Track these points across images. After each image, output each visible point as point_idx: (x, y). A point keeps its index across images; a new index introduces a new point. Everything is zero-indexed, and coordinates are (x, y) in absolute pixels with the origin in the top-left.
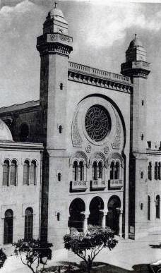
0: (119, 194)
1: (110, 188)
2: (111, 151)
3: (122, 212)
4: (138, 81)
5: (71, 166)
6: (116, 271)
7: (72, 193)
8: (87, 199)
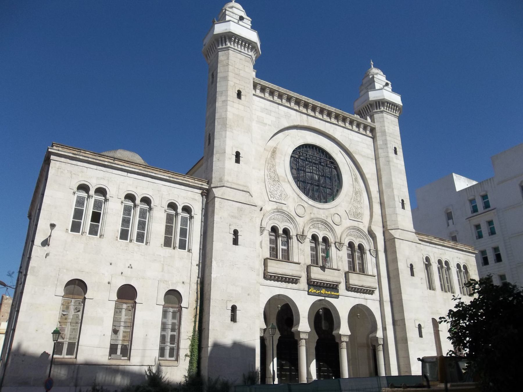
0: (371, 303)
1: (349, 288)
2: (347, 223)
3: (381, 342)
4: (383, 117)
5: (266, 233)
6: (351, 367)
7: (269, 282)
8: (304, 302)
